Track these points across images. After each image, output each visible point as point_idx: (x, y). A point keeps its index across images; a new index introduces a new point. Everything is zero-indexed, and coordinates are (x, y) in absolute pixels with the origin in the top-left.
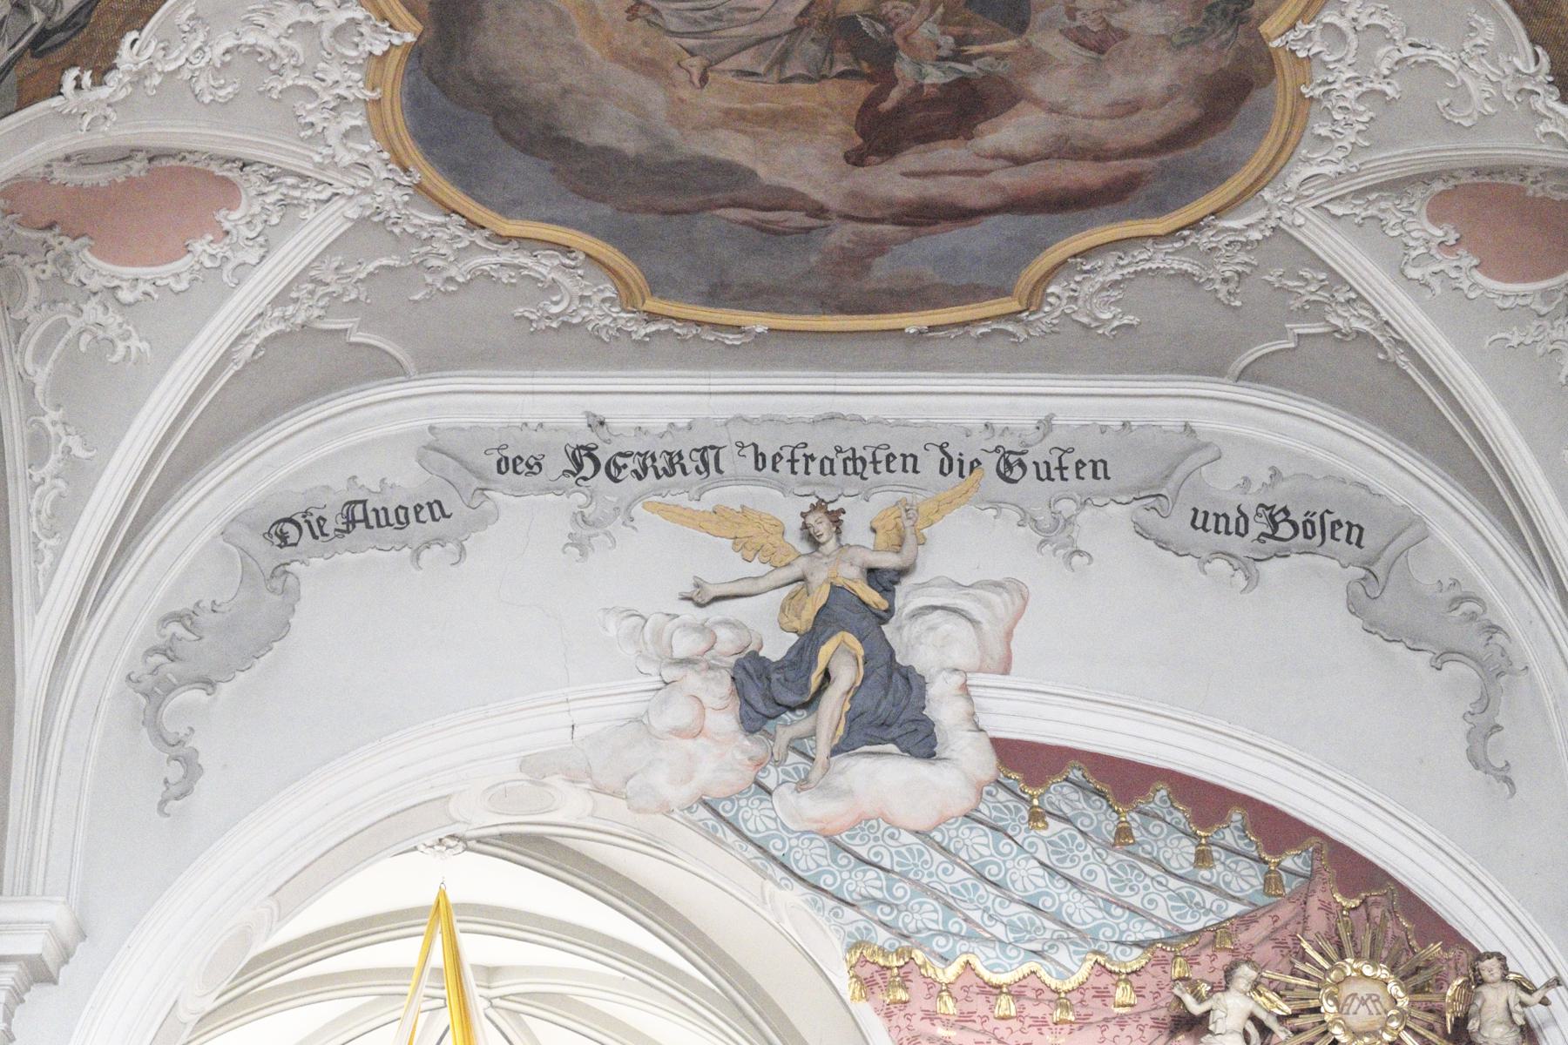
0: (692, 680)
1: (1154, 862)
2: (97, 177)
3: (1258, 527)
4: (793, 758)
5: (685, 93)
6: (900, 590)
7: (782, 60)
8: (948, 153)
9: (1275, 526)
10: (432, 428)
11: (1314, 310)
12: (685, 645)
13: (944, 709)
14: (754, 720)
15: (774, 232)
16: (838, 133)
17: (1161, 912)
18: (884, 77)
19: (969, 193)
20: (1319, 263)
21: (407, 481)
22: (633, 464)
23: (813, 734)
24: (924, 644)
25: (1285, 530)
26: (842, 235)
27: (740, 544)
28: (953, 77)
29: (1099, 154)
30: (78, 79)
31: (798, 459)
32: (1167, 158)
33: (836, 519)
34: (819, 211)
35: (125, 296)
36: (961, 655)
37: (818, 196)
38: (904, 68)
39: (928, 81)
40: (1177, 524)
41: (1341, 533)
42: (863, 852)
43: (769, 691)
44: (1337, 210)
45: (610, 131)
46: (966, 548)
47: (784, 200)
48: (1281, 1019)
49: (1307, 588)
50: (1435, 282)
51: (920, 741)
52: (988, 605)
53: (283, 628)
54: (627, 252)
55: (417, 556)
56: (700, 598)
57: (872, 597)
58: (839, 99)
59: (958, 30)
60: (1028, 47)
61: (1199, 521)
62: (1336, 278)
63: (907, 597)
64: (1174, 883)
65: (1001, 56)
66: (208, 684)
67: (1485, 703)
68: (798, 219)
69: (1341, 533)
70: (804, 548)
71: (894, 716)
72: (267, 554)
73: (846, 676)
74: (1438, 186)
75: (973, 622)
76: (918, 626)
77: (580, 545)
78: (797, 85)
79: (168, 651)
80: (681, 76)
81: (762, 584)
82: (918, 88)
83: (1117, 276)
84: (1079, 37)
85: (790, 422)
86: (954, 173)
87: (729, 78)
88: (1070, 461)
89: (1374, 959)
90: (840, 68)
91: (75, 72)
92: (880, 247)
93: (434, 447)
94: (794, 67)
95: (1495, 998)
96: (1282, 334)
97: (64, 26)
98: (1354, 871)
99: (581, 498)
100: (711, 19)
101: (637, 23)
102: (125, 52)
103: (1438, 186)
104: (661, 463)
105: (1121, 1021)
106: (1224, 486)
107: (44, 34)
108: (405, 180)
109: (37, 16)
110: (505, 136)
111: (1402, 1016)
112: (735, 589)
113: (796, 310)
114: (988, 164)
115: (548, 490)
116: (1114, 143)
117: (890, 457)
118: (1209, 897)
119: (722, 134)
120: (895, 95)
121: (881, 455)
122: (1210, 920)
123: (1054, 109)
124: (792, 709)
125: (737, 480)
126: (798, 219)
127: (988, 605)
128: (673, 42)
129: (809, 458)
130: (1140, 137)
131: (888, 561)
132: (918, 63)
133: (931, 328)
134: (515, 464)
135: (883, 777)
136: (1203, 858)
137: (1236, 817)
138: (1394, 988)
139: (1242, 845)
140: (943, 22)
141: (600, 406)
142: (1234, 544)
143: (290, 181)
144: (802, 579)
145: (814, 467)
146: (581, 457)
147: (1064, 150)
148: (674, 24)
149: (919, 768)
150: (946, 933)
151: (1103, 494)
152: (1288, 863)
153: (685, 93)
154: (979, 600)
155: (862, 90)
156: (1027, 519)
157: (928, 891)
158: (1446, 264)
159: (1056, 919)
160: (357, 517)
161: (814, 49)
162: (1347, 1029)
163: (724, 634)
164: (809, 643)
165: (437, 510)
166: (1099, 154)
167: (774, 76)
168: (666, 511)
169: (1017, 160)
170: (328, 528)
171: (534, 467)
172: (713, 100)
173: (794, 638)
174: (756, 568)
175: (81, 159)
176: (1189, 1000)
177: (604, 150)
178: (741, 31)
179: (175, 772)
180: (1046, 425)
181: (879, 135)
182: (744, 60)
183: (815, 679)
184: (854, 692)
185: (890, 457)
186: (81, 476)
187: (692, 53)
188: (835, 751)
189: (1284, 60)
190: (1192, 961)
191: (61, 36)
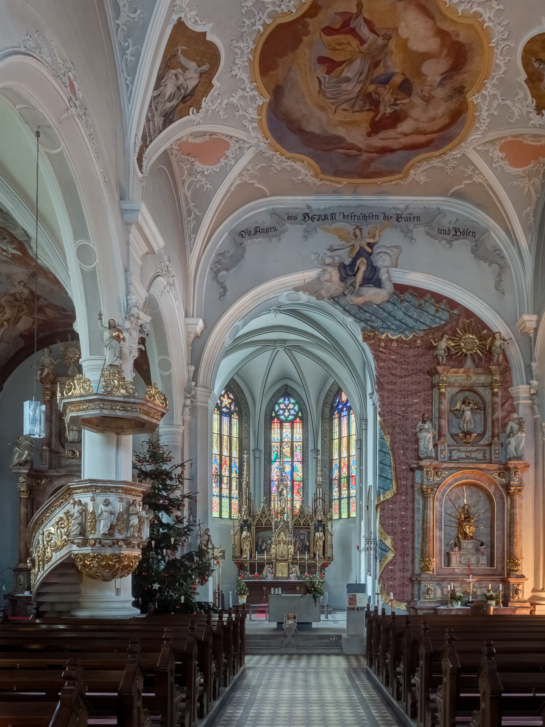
0: (330, 269)
1: (427, 312)
2: (198, 141)
3: (453, 233)
4: (351, 287)
5: (331, 116)
6: (374, 248)
7: (353, 106)
8: (390, 133)
9: (456, 233)
10: (273, 209)
11: (470, 177)
12: (328, 261)
13: (384, 277)
15: (348, 156)
16: (365, 127)
17: (427, 323)
18: (377, 111)
19: (394, 144)
20: (473, 164)
21: (268, 222)
22: (317, 217)
23: (355, 282)
24: (382, 261)
25: (458, 234)
26: (365, 157)
27: (340, 237)
28: (393, 111)
29: (425, 133)
30: (193, 110)
31: (352, 216)
32: (441, 134)
33: (361, 230)
34: (359, 150)
35: (206, 173)
36: (387, 263)
37: (360, 145)
38: (381, 108)
39: (387, 112)
40: (435, 232)
41: (471, 234)
42: (365, 309)
44: (478, 148)
45: (313, 127)
46: (389, 238)
47: (352, 147)
48: (452, 347)
49: (462, 249)
50: (499, 168)
51: (378, 284)
52: (393, 251)
53: (242, 257)
54: (316, 162)
55: (270, 240)
56: (331, 250)
57: (369, 250)
58: (365, 117)
59: (395, 96)
60: (411, 101)
61: (440, 231)
62: (476, 168)
63: (376, 250)
64: (431, 317)
65: (405, 104)
66: (227, 270)
67: (499, 275)
68: (355, 152)
69: (471, 234)
70: (354, 238)
71: (373, 279)
72: (239, 239)
73: (363, 268)
74: (503, 141)
75: (390, 256)
76: (378, 257)
77: (305, 237)
78: (357, 114)
79: (218, 262)
80: (329, 111)
81: (345, 246)
82: (385, 114)
83: (425, 168)
84: (424, 98)
85: (351, 207)
86: (391, 139)
87: (341, 111)
88: (412, 217)
89: (472, 334)
90: (367, 108)
91: (192, 108)
92: (372, 160)
93: (273, 213)
94: (356, 108)
95: (498, 343)
96: (461, 184)
97: (188, 95)
98: (469, 314)
99: (305, 226)
100: (338, 94)
101: (321, 95)
102: (203, 104)
103: (503, 141)
104: (323, 217)
105: (418, 347)
106: (446, 223)
107: (184, 97)
108: (267, 142)
109: (183, 91)
110: (290, 129)
111: (478, 347)
112: (338, 248)
113: (353, 178)
114: (399, 136)
115: (298, 224)
116: (429, 130)
117: (373, 216)
118: (438, 320)
119: (339, 128)
120: (379, 116)
121: (371, 215)
122: (438, 325)
123: (416, 120)
124: (350, 276)
125: (339, 221)
126: (355, 152)
127: (393, 251)
128: (328, 101)
129: (355, 216)
130: (435, 128)
131: (371, 241)
132: (385, 106)
133: (383, 182)
134: (292, 218)
135: (372, 294)
136: (437, 311)
137: (444, 301)
138: (476, 340)
139: (445, 308)
140: (392, 94)
142: (447, 237)
143: (241, 142)
144: (353, 245)
145: (356, 218)
146: (306, 216)
147: (417, 132)
148: (329, 95)
149: (378, 290)
150: (382, 328)
151: (419, 225)
152: (455, 312)
153: (331, 116)
154: (391, 250)
155: (372, 114)
156: (402, 231)
157: (378, 318)
158: (502, 163)
159: (405, 324)
160: (258, 231)
161: (361, 103)
162: (466, 349)
163: (336, 258)
164: (355, 260)
165: (275, 229)
166: (425, 133)
167: (351, 111)
168: (325, 230)
169: (406, 135)
170: (252, 233)
171: (295, 218)
172: (337, 118)
173: (351, 259)
174: (343, 243)
175: (194, 135)
176: (433, 342)
177: (312, 133)
178: (344, 97)
179: (221, 290)
180: (407, 207)
181: (376, 127)
182: (344, 106)
183: (356, 268)
184: (365, 273)
185: (373, 216)
186: (199, 220)
187: (333, 104)
188: (360, 286)
189: (470, 105)
190: (433, 334)
191: (188, 98)
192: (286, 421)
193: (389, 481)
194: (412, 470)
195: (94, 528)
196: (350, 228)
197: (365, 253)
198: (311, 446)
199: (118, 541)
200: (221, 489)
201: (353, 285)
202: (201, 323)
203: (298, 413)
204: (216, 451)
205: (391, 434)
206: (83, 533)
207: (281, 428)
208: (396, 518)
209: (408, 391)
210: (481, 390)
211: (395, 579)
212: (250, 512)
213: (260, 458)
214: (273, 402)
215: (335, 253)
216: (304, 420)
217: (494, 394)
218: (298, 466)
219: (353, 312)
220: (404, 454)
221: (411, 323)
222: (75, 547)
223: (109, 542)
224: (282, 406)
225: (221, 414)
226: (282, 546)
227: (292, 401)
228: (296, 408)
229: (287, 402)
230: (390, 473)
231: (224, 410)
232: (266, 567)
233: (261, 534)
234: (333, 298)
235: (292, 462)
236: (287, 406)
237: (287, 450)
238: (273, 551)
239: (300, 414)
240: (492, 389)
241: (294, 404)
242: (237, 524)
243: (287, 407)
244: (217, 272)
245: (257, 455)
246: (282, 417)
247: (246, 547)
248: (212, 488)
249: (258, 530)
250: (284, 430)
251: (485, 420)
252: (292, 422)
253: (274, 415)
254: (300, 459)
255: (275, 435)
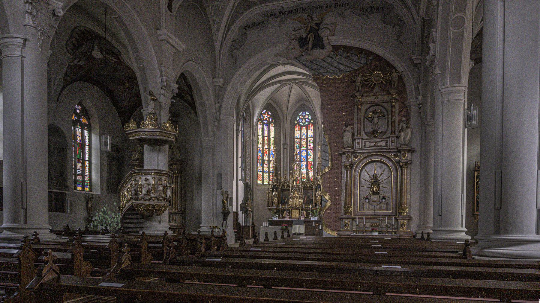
12: (293, 37)
13: (326, 42)
14: (301, 47)
24: (324, 33)
25: (373, 10)
43: (303, 42)
51: (323, 47)
61: (361, 10)
71: (319, 44)
79: (233, 45)
89: (379, 71)
98: (379, 58)
135: (318, 53)
136: (358, 59)
141: (283, 5)
146: (281, 13)
157: (322, 67)
160: (254, 25)
188: (312, 49)
192: (304, 126)
193: (327, 162)
194: (341, 155)
195: (141, 192)
196: (305, 15)
197: (315, 30)
198: (318, 140)
199: (152, 198)
200: (263, 167)
201: (307, 49)
202: (221, 80)
203: (310, 120)
204: (260, 146)
205: (329, 135)
206: (136, 194)
207: (301, 130)
208: (332, 183)
209: (339, 108)
210: (385, 104)
211: (331, 218)
212: (277, 179)
213: (287, 149)
214: (295, 115)
215: (297, 32)
216: (314, 124)
217: (393, 107)
218: (311, 152)
219: (307, 65)
220: (337, 146)
221: (341, 67)
222: (134, 201)
223: (147, 198)
224: (301, 117)
225: (264, 124)
226: (297, 200)
227: (307, 113)
228: (310, 118)
229: (304, 114)
230: (329, 157)
231: (265, 122)
232: (285, 212)
233: (285, 193)
234: (296, 58)
235: (307, 149)
236: (304, 117)
237: (303, 143)
238: (290, 203)
239: (312, 121)
240: (391, 103)
241: (308, 115)
242: (270, 187)
243: (304, 117)
244: (232, 51)
245: (286, 147)
246: (301, 124)
247: (275, 200)
248: (257, 167)
249: (282, 190)
250: (303, 131)
251: (388, 123)
252: (307, 127)
253: (296, 122)
254: (312, 148)
255: (297, 134)
